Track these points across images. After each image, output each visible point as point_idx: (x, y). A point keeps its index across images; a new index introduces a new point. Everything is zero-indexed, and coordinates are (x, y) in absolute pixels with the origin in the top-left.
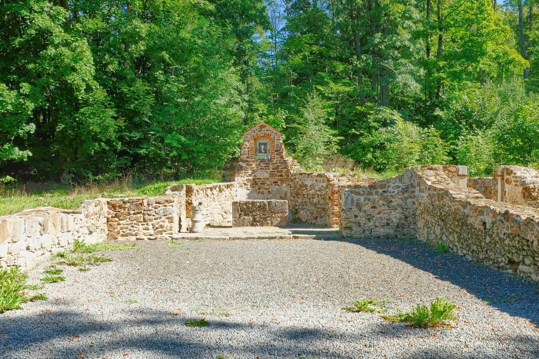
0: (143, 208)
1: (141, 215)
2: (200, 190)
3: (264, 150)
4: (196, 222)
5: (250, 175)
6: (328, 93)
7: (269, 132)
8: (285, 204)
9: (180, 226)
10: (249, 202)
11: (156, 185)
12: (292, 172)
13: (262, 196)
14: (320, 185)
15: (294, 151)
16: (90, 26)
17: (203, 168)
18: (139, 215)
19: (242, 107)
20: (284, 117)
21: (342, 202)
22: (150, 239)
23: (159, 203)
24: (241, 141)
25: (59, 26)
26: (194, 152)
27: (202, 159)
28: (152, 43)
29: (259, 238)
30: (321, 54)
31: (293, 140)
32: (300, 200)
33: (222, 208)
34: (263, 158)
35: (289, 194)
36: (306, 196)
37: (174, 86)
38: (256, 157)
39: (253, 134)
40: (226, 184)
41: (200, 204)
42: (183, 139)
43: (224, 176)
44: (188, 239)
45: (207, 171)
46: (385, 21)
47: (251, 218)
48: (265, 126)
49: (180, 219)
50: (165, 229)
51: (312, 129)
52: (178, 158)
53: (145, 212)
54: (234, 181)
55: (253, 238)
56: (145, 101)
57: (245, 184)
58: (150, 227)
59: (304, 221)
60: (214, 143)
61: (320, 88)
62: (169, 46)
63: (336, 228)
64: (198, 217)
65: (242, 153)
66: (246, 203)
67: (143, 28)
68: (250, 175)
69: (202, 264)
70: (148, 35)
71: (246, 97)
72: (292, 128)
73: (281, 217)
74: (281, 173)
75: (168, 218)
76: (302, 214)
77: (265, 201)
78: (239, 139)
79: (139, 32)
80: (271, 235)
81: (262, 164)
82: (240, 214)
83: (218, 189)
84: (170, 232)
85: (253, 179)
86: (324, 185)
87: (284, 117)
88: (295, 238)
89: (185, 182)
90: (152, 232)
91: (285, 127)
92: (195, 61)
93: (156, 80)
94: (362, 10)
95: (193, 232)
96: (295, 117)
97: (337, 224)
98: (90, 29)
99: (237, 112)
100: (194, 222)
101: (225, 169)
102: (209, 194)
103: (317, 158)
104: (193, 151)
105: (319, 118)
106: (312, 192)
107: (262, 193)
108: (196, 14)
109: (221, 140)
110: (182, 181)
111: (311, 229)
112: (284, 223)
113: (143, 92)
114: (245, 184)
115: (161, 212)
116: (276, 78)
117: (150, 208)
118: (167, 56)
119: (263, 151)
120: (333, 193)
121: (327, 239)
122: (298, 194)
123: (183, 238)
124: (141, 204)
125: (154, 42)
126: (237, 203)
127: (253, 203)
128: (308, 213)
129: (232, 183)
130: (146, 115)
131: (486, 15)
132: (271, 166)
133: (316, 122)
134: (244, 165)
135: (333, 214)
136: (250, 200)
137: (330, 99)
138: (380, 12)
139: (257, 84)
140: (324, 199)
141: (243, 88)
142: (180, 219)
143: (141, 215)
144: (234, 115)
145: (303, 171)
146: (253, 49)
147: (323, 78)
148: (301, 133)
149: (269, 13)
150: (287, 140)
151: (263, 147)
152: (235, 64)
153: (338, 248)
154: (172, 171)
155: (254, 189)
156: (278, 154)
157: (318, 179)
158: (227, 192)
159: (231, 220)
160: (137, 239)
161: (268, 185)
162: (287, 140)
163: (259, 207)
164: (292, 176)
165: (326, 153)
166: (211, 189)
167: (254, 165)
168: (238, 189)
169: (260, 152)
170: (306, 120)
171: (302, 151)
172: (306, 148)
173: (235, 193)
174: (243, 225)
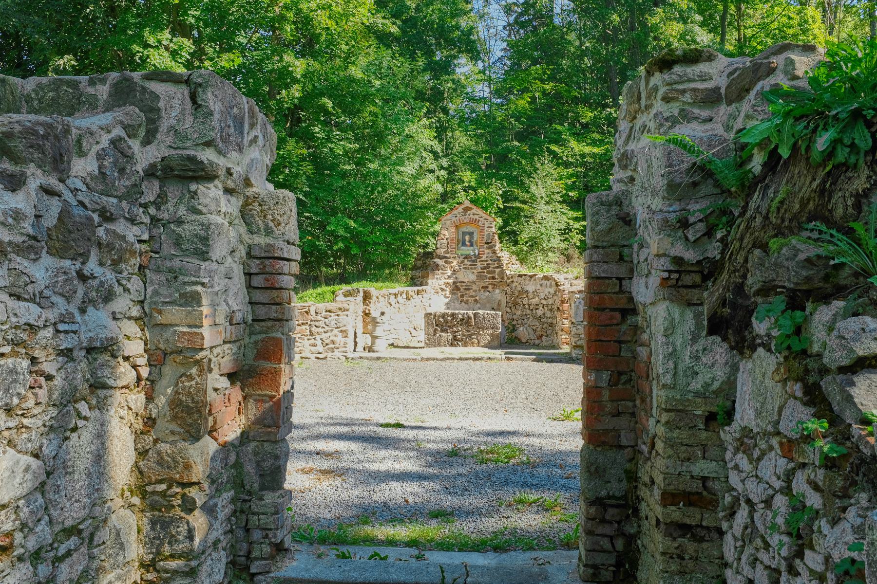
0: (310, 317)
1: (307, 327)
2: (380, 297)
3: (470, 241)
4: (377, 337)
5: (449, 277)
6: (567, 156)
7: (476, 217)
8: (497, 318)
9: (356, 344)
10: (447, 314)
11: (319, 290)
12: (508, 272)
13: (466, 306)
14: (547, 290)
15: (516, 243)
16: (224, 64)
17: (382, 266)
18: (304, 327)
19: (438, 177)
20: (501, 192)
21: (572, 312)
22: (318, 358)
23: (330, 311)
24: (437, 228)
25: (181, 66)
26: (369, 243)
27: (379, 254)
28: (310, 86)
29: (461, 359)
30: (558, 96)
31: (514, 226)
32: (519, 313)
33: (411, 322)
34: (467, 253)
35: (504, 304)
36: (527, 306)
37: (342, 145)
38: (458, 252)
39: (454, 219)
40: (416, 288)
41: (383, 314)
42: (352, 224)
43: (412, 279)
44: (367, 358)
45: (387, 271)
46: (654, 48)
47: (450, 336)
48: (470, 209)
49: (355, 333)
50: (337, 345)
51: (542, 211)
52: (346, 252)
53: (312, 323)
54: (427, 284)
55: (453, 359)
56: (299, 170)
57: (442, 290)
58: (319, 342)
59: (524, 341)
60: (397, 232)
61: (554, 148)
62: (332, 91)
63: (566, 349)
64: (378, 332)
65: (438, 246)
66: (444, 316)
67: (299, 66)
68: (449, 277)
69: (389, 382)
70: (304, 76)
71: (445, 162)
72: (513, 208)
73: (492, 335)
74: (493, 275)
75: (341, 331)
76: (522, 332)
77: (470, 313)
78: (433, 224)
79: (292, 72)
80: (476, 356)
81: (466, 262)
82: (436, 329)
83: (404, 296)
84: (344, 349)
85: (454, 283)
86: (552, 291)
87: (501, 192)
88: (508, 359)
89: (363, 285)
90: (320, 348)
91: (502, 207)
92: (371, 112)
93: (312, 137)
94: (620, 30)
95: (373, 351)
96: (516, 191)
97: (568, 344)
98: (223, 68)
99: (431, 185)
100: (374, 338)
101: (415, 268)
102: (393, 303)
103: (550, 254)
104: (367, 243)
105: (553, 193)
106: (535, 301)
107: (467, 302)
108: (373, 42)
109: (408, 227)
110: (355, 285)
111: (532, 351)
112: (496, 343)
113: (297, 156)
114: (442, 290)
115: (333, 322)
116: (490, 130)
117: (319, 317)
118: (329, 104)
119: (468, 243)
120: (563, 302)
121: (552, 361)
122: (515, 304)
123: (361, 358)
124: (307, 312)
125: (313, 85)
126: (431, 314)
127: (453, 315)
128: (530, 331)
129: (424, 287)
130: (301, 190)
131: (811, 37)
132: (479, 264)
133: (547, 199)
134: (440, 262)
135: (562, 330)
136: (450, 312)
137: (567, 165)
138: (647, 35)
139: (462, 140)
140: (551, 310)
141: (438, 148)
142: (355, 333)
143: (307, 327)
144: (427, 189)
145: (524, 271)
146: (455, 90)
147: (560, 133)
148: (526, 216)
149: (481, 32)
150: (504, 226)
151: (467, 238)
152: (429, 114)
153: (561, 370)
154: (335, 270)
155: (455, 297)
156: (489, 248)
157: (544, 282)
158: (417, 299)
159: (423, 339)
160: (302, 358)
161: (475, 291)
162: (504, 226)
163: (462, 320)
164: (508, 278)
165: (563, 245)
166: (396, 295)
167: (455, 263)
168: (433, 297)
169: (464, 244)
170: (533, 197)
171: (526, 243)
172: (532, 239)
173: (429, 302)
174: (439, 345)
